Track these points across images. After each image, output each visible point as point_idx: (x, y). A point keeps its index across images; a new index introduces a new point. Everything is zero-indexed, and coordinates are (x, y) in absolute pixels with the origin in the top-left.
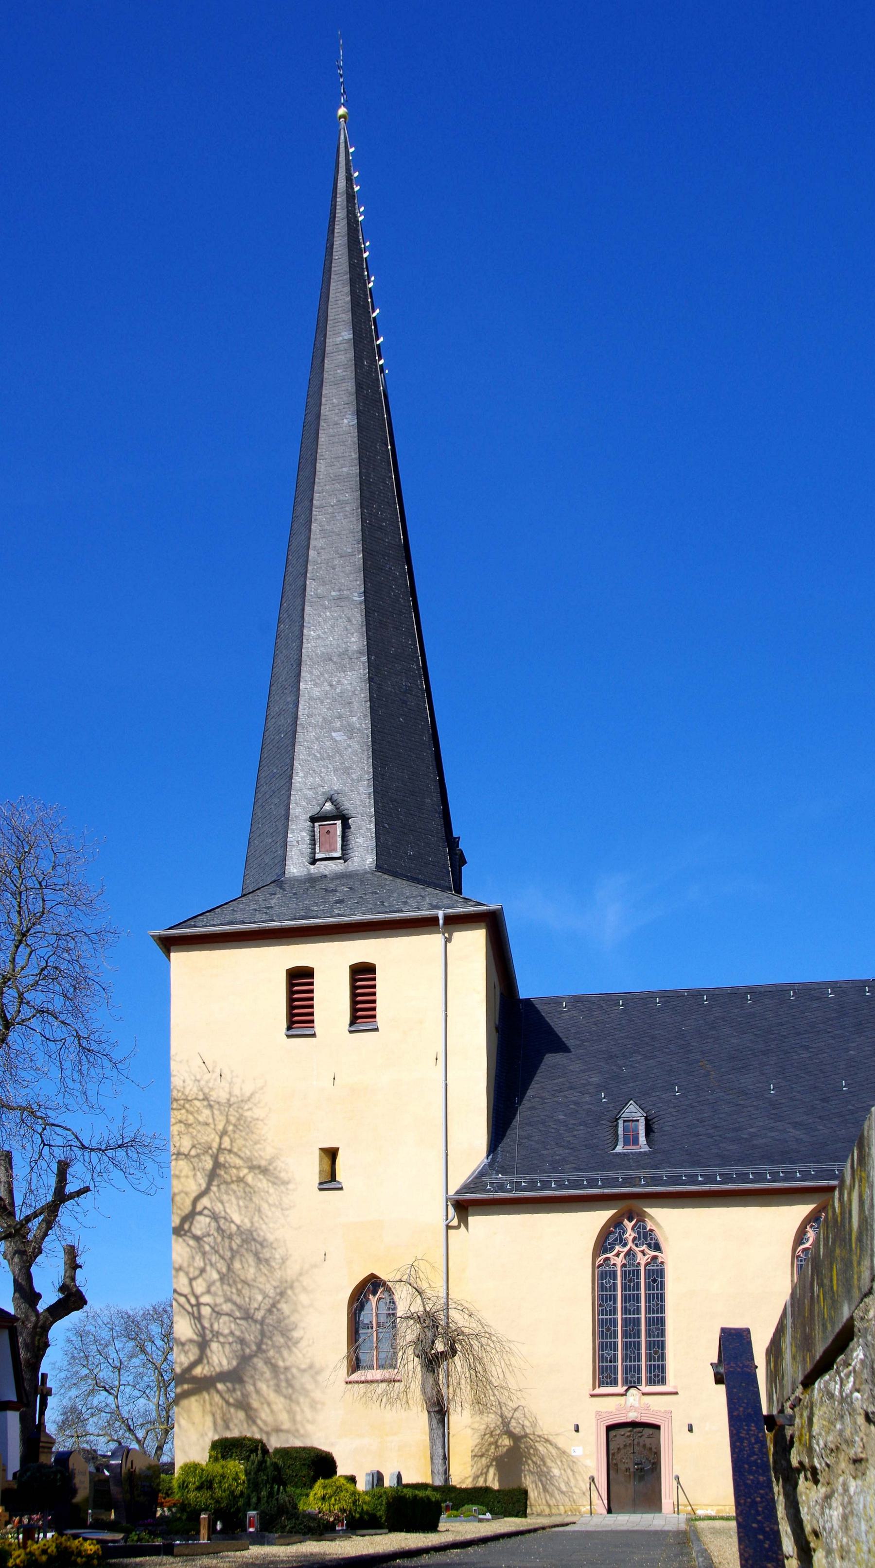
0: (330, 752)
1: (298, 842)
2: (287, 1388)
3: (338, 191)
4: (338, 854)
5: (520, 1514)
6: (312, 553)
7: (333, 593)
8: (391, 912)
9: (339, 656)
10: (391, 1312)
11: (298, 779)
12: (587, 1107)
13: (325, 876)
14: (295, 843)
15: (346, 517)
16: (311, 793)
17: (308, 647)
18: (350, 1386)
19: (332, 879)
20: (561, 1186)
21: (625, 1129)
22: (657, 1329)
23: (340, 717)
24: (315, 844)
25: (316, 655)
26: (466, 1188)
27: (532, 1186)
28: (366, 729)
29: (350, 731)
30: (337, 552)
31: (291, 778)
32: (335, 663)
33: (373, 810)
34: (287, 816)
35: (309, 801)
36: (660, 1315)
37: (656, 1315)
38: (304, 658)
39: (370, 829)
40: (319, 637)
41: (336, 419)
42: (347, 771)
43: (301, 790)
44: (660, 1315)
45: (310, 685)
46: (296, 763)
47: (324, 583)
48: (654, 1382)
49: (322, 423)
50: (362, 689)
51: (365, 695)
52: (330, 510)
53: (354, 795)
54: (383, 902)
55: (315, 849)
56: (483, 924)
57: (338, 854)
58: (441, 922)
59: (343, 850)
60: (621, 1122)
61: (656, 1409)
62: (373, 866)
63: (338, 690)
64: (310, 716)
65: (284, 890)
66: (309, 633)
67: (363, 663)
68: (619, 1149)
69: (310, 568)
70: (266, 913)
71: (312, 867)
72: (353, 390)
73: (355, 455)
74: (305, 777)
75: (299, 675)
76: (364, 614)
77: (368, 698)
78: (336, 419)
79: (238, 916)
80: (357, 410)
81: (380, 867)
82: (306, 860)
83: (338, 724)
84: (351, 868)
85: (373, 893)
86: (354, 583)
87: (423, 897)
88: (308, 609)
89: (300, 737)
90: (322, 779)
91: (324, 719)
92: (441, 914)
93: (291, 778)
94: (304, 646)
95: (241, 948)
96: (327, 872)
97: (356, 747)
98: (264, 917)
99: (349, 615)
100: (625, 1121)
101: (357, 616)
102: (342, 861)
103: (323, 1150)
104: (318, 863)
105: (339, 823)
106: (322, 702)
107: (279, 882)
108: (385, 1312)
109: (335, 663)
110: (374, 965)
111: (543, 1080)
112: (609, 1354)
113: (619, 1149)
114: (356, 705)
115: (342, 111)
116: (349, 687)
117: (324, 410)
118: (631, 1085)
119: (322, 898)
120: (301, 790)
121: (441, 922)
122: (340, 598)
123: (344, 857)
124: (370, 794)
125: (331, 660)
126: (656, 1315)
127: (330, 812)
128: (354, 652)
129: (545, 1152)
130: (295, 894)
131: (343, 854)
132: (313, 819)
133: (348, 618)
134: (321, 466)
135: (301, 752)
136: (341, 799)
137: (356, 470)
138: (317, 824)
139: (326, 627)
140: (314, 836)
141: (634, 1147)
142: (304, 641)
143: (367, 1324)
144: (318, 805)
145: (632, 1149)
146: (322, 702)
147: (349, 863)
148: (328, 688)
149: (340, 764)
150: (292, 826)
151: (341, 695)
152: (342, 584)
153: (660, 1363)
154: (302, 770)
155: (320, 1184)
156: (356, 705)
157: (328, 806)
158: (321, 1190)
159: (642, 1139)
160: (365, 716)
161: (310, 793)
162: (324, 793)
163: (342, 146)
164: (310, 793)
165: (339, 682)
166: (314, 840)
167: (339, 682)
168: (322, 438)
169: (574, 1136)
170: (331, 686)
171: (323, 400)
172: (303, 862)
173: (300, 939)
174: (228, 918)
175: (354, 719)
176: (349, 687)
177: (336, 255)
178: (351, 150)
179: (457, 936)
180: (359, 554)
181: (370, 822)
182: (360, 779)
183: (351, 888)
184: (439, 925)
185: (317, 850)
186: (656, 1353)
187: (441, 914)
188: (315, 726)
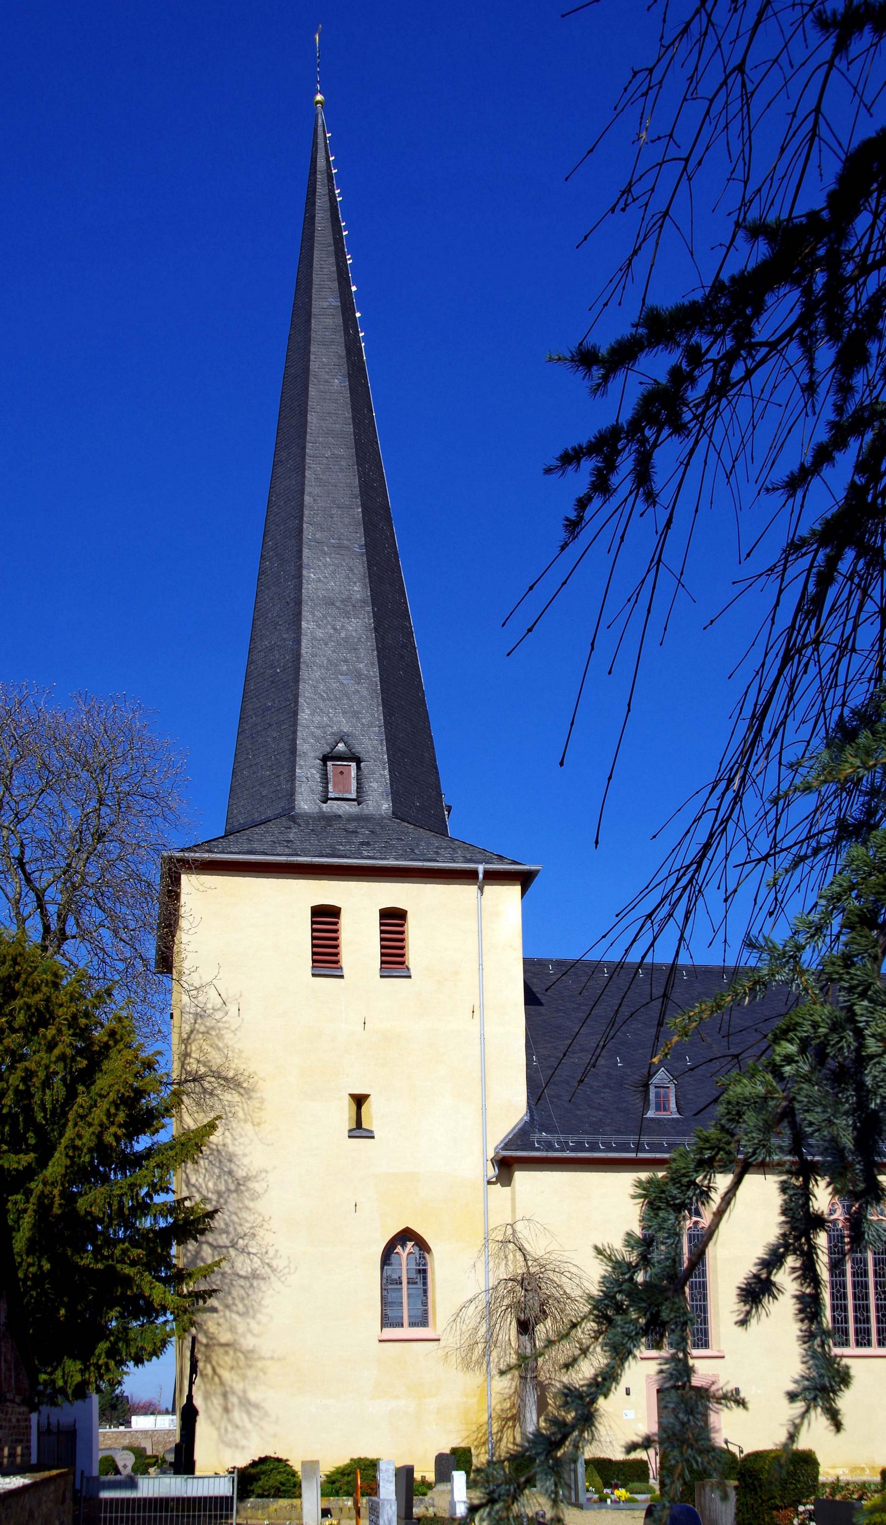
0: (337, 693)
1: (307, 778)
2: (819, 1346)
3: (318, 169)
4: (354, 796)
5: (374, 1486)
6: (307, 499)
7: (333, 541)
8: (424, 860)
9: (342, 601)
10: (421, 1267)
11: (304, 716)
12: (606, 1070)
13: (340, 816)
14: (304, 779)
15: (341, 470)
16: (319, 732)
17: (308, 589)
18: (383, 1344)
19: (348, 820)
20: (609, 1149)
21: (657, 1095)
22: (699, 1293)
23: (346, 661)
24: (327, 783)
25: (318, 597)
26: (508, 1144)
27: (579, 1147)
28: (375, 677)
29: (358, 676)
30: (333, 502)
31: (297, 715)
32: (338, 608)
33: (386, 756)
34: (293, 751)
35: (317, 739)
36: (702, 1280)
37: (698, 1280)
38: (304, 597)
39: (384, 776)
40: (319, 580)
41: (327, 377)
42: (356, 714)
43: (308, 727)
44: (702, 1280)
45: (312, 625)
46: (301, 700)
47: (322, 530)
48: (861, 1345)
49: (312, 378)
50: (367, 638)
51: (371, 643)
52: (325, 461)
53: (365, 740)
54: (413, 851)
55: (327, 787)
56: (519, 883)
57: (354, 796)
58: (481, 876)
59: (358, 792)
60: (652, 1090)
61: (705, 1372)
62: (390, 812)
63: (343, 635)
64: (314, 655)
65: (300, 825)
66: (309, 575)
67: (368, 613)
68: (651, 1114)
69: (306, 512)
70: (287, 846)
71: (324, 805)
72: (344, 353)
73: (349, 415)
74: (312, 714)
75: (299, 614)
76: (366, 565)
77: (375, 647)
78: (327, 377)
79: (256, 846)
80: (349, 373)
81: (398, 814)
82: (317, 797)
83: (345, 668)
84: (366, 812)
85: (398, 839)
86: (354, 535)
87: (454, 849)
88: (306, 552)
89: (304, 673)
90: (331, 719)
91: (329, 660)
92: (481, 868)
93: (296, 713)
94: (305, 586)
95: (244, 877)
96: (340, 812)
97: (365, 693)
98: (287, 851)
99: (351, 565)
100: (656, 1087)
101: (360, 567)
102: (355, 803)
103: (353, 1096)
104: (329, 802)
105: (353, 764)
106: (326, 644)
107: (289, 815)
108: (414, 1267)
109: (338, 608)
110: (406, 912)
111: (553, 1040)
112: (840, 1315)
113: (651, 1114)
114: (362, 652)
115: (319, 97)
116: (354, 634)
117: (314, 366)
118: (640, 1051)
119: (345, 837)
120: (308, 727)
121: (481, 876)
122: (340, 547)
123: (359, 800)
124: (382, 740)
125: (333, 604)
126: (698, 1280)
127: (344, 753)
128: (358, 601)
129: (578, 1112)
130: (312, 830)
131: (358, 797)
132: (325, 759)
133: (350, 567)
134: (312, 418)
135: (306, 690)
136: (351, 741)
137: (350, 428)
138: (329, 763)
139: (327, 572)
140: (326, 774)
141: (665, 1113)
142: (304, 581)
143: (395, 1280)
144: (328, 744)
145: (662, 1115)
146: (326, 644)
147: (363, 806)
148: (332, 631)
149: (350, 707)
150: (300, 762)
151: (345, 640)
152: (342, 534)
153: (703, 1326)
154: (308, 708)
155: (350, 1131)
156: (362, 652)
157: (341, 746)
158: (350, 1137)
159: (673, 1106)
160: (373, 664)
161: (318, 732)
162: (333, 734)
163: (320, 129)
164: (318, 732)
165: (343, 627)
166: (327, 779)
167: (343, 627)
168: (312, 392)
169: (603, 1098)
170: (335, 629)
171: (312, 357)
172: (315, 800)
173: (495, 882)
174: (246, 847)
175: (361, 666)
176: (354, 634)
177: (319, 227)
178: (328, 135)
179: (487, 888)
180: (358, 508)
181: (384, 769)
182: (371, 725)
183: (372, 832)
184: (478, 878)
185: (330, 788)
186: (699, 1316)
187: (481, 868)
188: (321, 666)
